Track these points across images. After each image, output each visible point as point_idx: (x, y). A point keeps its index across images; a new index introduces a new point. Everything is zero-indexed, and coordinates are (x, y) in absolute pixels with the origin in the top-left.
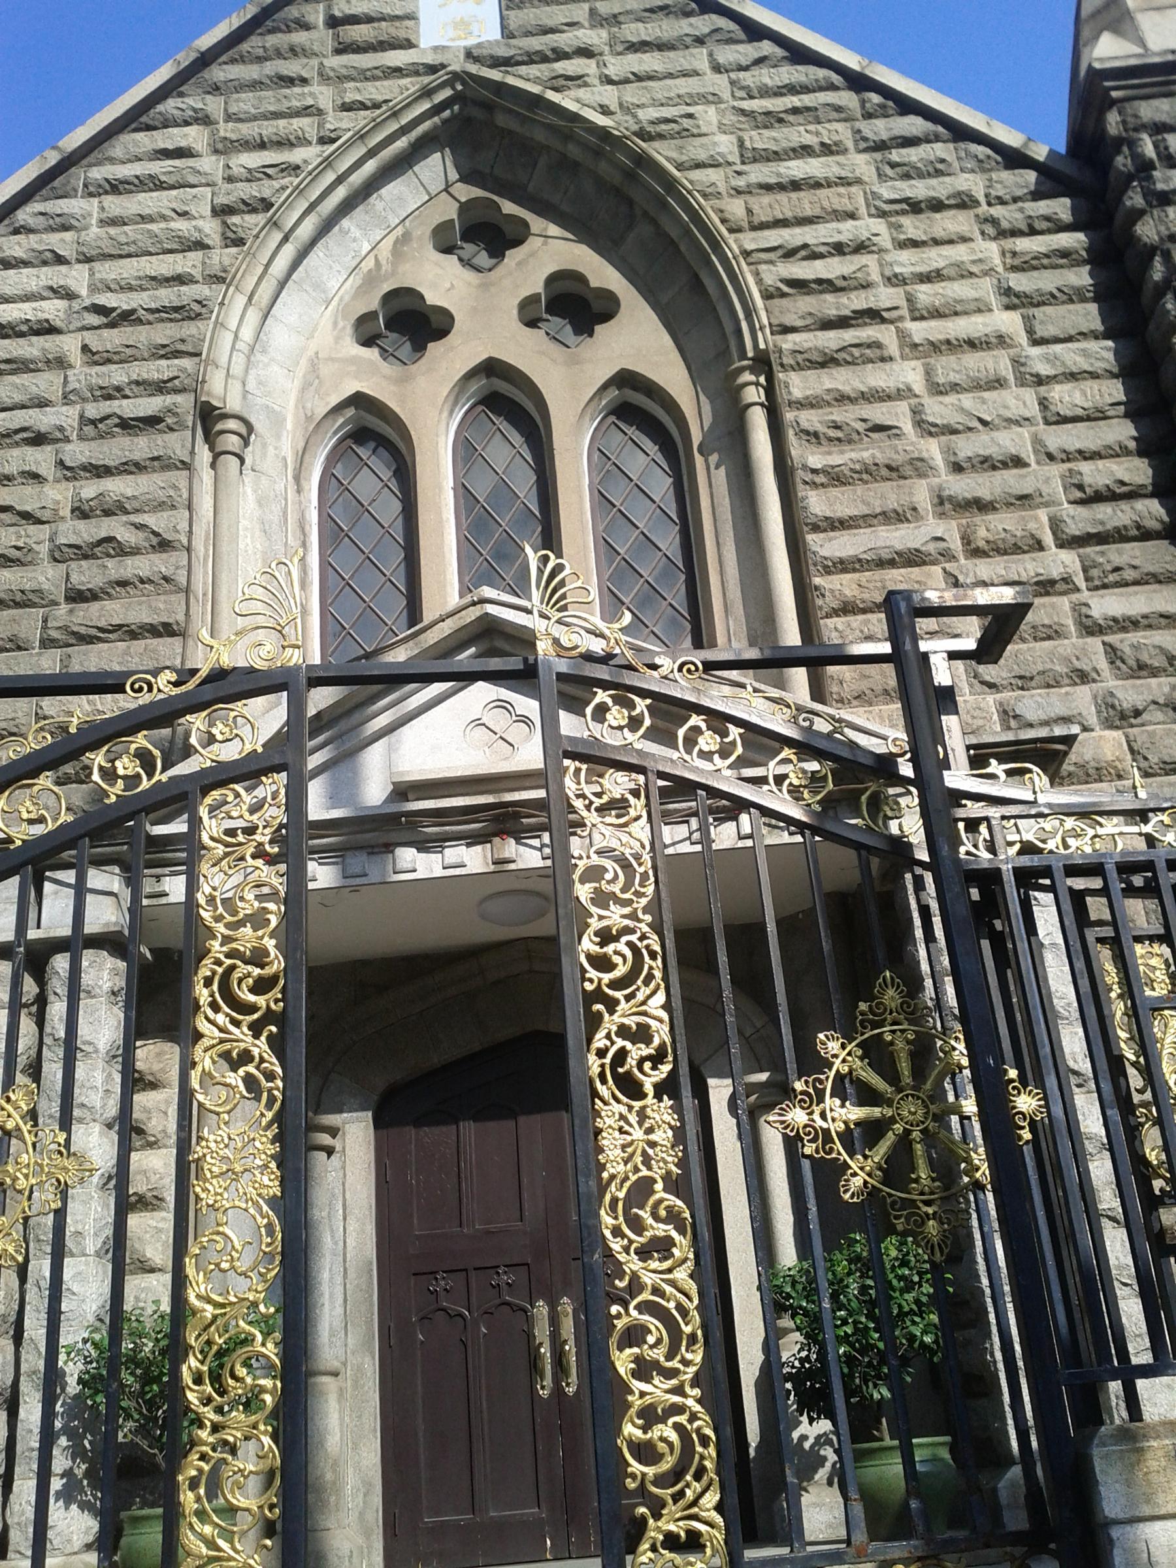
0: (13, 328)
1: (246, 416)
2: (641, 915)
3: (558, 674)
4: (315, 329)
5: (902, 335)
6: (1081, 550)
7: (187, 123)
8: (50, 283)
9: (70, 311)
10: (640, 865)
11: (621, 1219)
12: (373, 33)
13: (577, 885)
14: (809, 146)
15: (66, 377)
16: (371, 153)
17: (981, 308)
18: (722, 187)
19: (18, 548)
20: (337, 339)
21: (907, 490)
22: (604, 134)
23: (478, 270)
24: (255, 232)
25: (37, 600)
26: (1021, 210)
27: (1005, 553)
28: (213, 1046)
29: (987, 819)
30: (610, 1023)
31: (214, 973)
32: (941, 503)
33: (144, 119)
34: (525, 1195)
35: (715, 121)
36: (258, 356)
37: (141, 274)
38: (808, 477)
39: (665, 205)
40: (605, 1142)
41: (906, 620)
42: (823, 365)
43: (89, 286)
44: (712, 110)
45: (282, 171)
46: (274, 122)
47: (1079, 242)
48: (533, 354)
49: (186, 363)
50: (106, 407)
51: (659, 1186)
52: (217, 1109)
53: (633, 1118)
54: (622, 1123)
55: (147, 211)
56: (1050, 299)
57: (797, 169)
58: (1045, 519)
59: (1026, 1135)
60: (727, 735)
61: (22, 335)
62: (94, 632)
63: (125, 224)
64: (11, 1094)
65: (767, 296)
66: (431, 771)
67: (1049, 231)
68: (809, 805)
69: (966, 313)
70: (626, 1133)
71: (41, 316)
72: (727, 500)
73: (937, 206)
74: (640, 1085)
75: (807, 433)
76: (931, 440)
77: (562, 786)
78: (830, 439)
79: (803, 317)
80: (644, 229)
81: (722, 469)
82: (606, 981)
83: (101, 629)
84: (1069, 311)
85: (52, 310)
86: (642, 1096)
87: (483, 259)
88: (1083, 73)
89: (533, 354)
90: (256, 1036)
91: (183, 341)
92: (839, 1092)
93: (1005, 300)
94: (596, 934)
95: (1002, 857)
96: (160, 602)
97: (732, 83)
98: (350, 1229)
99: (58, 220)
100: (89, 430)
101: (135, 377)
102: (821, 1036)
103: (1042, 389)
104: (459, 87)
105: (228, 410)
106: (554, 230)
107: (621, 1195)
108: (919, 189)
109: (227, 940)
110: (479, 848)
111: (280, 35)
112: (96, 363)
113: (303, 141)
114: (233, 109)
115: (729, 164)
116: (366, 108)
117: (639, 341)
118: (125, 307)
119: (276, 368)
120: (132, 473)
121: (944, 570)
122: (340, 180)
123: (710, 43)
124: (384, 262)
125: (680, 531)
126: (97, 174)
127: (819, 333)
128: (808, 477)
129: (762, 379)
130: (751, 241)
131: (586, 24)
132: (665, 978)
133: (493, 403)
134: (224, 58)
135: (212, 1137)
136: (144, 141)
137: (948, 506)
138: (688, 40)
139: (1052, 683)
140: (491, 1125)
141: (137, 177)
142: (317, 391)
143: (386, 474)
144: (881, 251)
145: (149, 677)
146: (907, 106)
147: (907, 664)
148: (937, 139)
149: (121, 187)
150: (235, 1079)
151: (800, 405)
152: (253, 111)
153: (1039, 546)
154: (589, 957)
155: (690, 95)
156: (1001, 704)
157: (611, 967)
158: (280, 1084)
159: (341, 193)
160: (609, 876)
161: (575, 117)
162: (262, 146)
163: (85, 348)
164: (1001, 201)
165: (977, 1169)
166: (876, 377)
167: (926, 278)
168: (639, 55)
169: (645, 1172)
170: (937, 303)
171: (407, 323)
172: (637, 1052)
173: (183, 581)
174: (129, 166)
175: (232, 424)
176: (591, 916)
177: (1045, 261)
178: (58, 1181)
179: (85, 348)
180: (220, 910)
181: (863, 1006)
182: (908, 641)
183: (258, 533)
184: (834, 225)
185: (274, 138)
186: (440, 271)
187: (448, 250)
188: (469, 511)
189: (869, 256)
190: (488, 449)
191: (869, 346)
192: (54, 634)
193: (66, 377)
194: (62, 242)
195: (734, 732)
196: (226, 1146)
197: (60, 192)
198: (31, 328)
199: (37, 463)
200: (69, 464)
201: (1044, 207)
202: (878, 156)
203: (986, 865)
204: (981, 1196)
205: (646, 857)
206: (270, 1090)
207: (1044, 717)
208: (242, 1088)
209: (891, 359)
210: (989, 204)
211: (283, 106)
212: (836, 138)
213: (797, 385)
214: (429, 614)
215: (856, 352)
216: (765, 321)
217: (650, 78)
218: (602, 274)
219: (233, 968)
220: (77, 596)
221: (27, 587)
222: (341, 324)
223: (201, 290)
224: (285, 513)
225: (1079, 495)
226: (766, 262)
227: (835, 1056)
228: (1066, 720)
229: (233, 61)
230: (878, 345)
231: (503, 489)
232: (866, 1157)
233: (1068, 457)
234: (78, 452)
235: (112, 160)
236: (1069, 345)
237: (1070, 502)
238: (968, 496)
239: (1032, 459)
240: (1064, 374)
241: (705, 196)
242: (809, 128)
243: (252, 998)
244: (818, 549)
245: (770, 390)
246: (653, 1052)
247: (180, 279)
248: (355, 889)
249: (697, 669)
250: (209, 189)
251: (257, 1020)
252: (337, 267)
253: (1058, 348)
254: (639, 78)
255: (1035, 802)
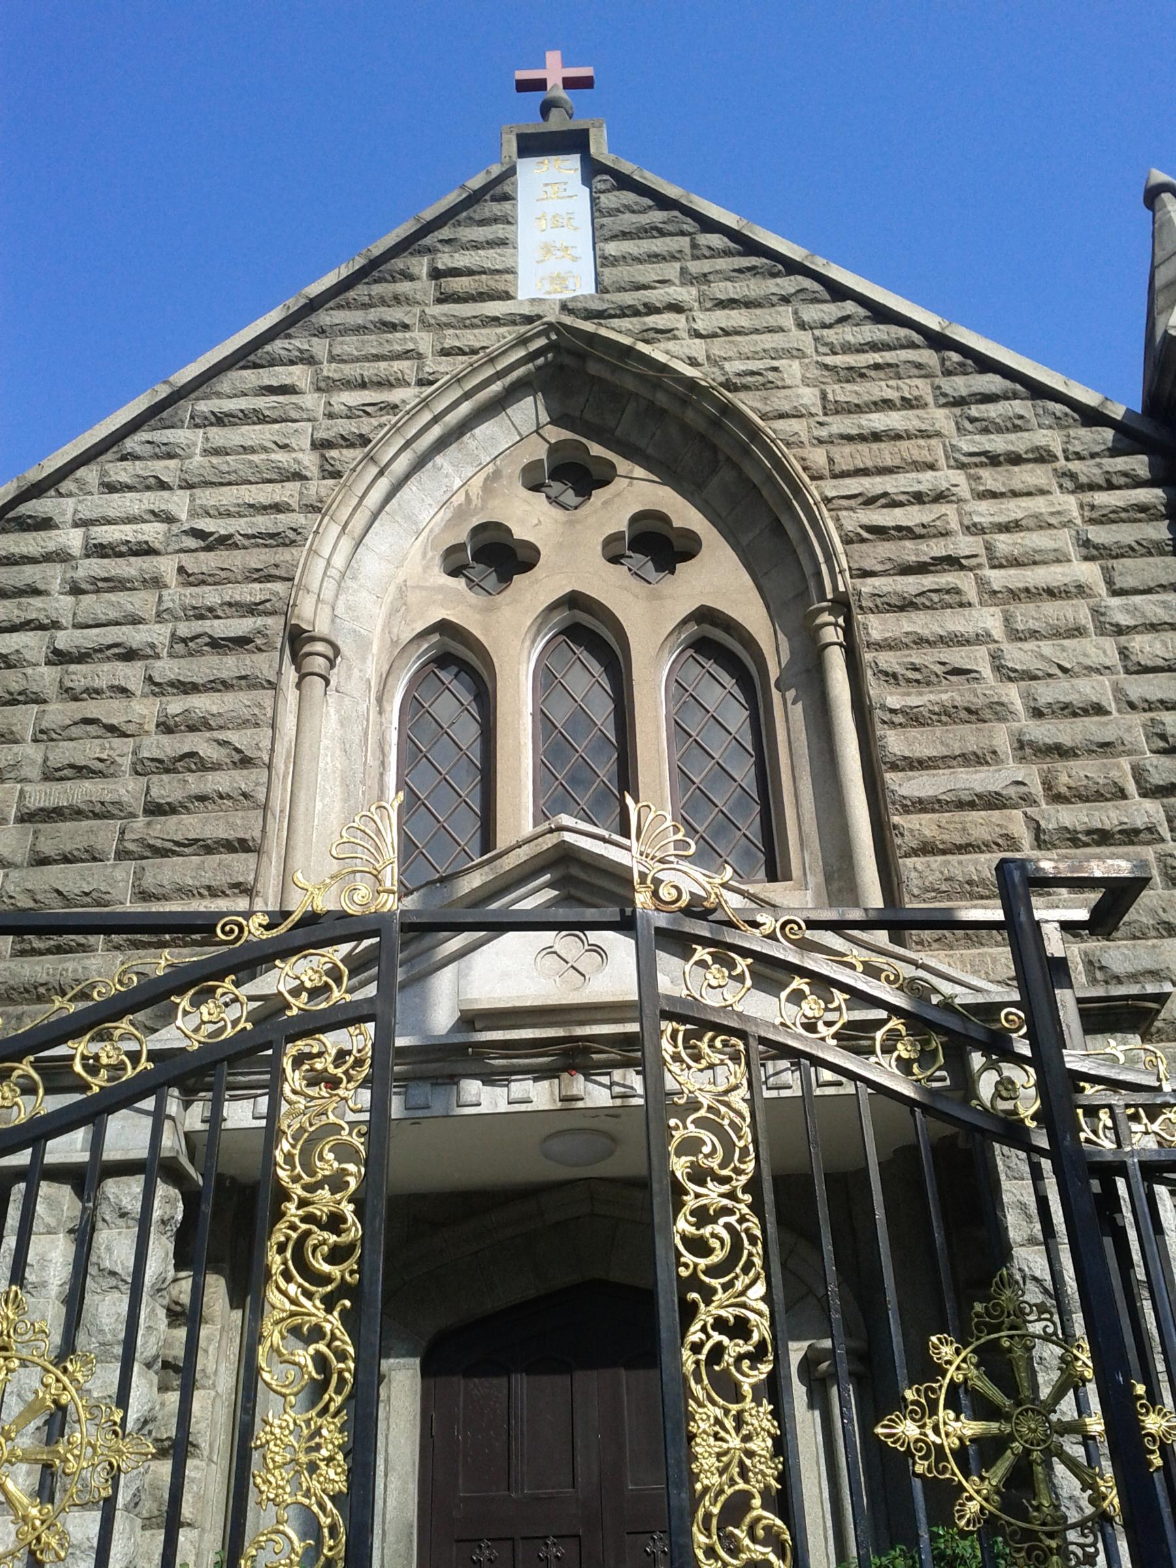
0: (113, 549)
1: (333, 638)
2: (740, 1195)
3: (657, 929)
4: (404, 558)
5: (981, 582)
6: (1165, 800)
7: (292, 363)
8: (152, 507)
9: (169, 535)
10: (740, 1138)
11: (715, 1537)
12: (474, 285)
13: (673, 1159)
14: (890, 400)
15: (160, 597)
16: (467, 396)
17: (1060, 559)
18: (804, 437)
19: (101, 760)
20: (426, 568)
21: (986, 733)
22: (692, 384)
23: (565, 507)
24: (352, 466)
25: (116, 812)
26: (1099, 465)
27: (1087, 800)
28: (283, 1320)
29: (1110, 1107)
30: (706, 1315)
31: (288, 1238)
32: (1022, 748)
33: (252, 358)
34: (579, 1459)
35: (799, 376)
36: (349, 583)
37: (240, 501)
38: (887, 717)
39: (747, 452)
40: (699, 1450)
41: (1020, 890)
42: (902, 609)
43: (189, 511)
44: (796, 364)
45: (381, 409)
46: (376, 364)
47: (1157, 497)
48: (617, 590)
49: (279, 587)
50: (198, 626)
51: (757, 1502)
52: (284, 1390)
53: (729, 1424)
54: (717, 1428)
55: (250, 443)
56: (1129, 551)
57: (878, 421)
58: (1128, 768)
59: (1157, 1460)
60: (832, 1001)
61: (121, 555)
62: (169, 845)
63: (227, 454)
64: (68, 1365)
65: (847, 541)
66: (500, 999)
67: (1127, 487)
68: (918, 1080)
69: (1045, 563)
70: (723, 1440)
71: (141, 538)
72: (804, 735)
73: (1015, 459)
74: (737, 1386)
75: (886, 674)
76: (1010, 685)
77: (658, 1048)
78: (909, 681)
79: (882, 562)
80: (727, 475)
81: (800, 705)
82: (702, 1267)
83: (177, 843)
84: (1148, 564)
85: (152, 532)
86: (738, 1398)
87: (570, 497)
88: (1158, 339)
89: (617, 590)
90: (329, 1310)
91: (276, 566)
92: (953, 1403)
93: (1084, 551)
94: (692, 1213)
95: (1128, 1149)
96: (238, 818)
97: (816, 339)
98: (391, 1487)
99: (163, 448)
100: (180, 648)
101: (228, 599)
102: (934, 1339)
103: (1123, 638)
104: (554, 337)
105: (316, 633)
106: (639, 472)
107: (715, 1510)
108: (998, 443)
109: (303, 1203)
110: (545, 1084)
111: (385, 285)
112: (191, 584)
113: (402, 382)
114: (337, 350)
115: (812, 415)
116: (464, 354)
117: (720, 579)
118: (223, 532)
119: (365, 594)
120: (219, 691)
121: (1025, 814)
122: (436, 420)
123: (796, 303)
124: (474, 498)
125: (755, 763)
126: (203, 407)
127: (898, 578)
128: (887, 717)
129: (841, 621)
130: (831, 488)
131: (677, 282)
132: (766, 1266)
133: (575, 633)
134: (331, 304)
135: (276, 1422)
136: (251, 378)
137: (1028, 751)
138: (775, 299)
139: (1138, 934)
140: (545, 1380)
141: (242, 411)
142: (404, 618)
143: (467, 698)
144: (960, 500)
145: (240, 919)
146: (986, 365)
147: (1019, 931)
148: (1015, 396)
149: (226, 420)
150: (304, 1356)
151: (879, 646)
152: (356, 353)
153: (1122, 794)
154: (684, 1238)
155: (775, 350)
156: (1086, 954)
157: (709, 1251)
158: (352, 1365)
159: (436, 431)
160: (706, 1149)
161: (664, 368)
162: (363, 385)
163: (181, 570)
164: (1079, 457)
165: (1104, 1498)
166: (954, 622)
167: (1005, 528)
168: (727, 311)
169: (741, 1485)
170: (1016, 552)
171: (495, 556)
172: (735, 1347)
173: (262, 797)
174: (234, 400)
175: (320, 647)
176: (687, 1193)
177: (1123, 515)
178: (111, 1464)
179: (181, 570)
180: (299, 1169)
181: (979, 1307)
182: (1022, 911)
183: (338, 752)
184: (914, 475)
185: (375, 379)
186: (528, 508)
187: (536, 488)
188: (546, 738)
189: (948, 506)
190: (567, 677)
191: (948, 592)
192: (131, 846)
193: (160, 597)
194: (167, 469)
195: (839, 997)
196: (291, 1433)
197: (168, 423)
198: (130, 549)
199: (127, 678)
200: (158, 680)
201: (1121, 463)
202: (957, 411)
203: (1110, 1158)
204: (1110, 1530)
205: (746, 1131)
206: (340, 1372)
207: (1131, 970)
208: (311, 1368)
209: (970, 605)
210: (1067, 459)
211: (385, 350)
212: (916, 393)
213: (876, 627)
214: (503, 840)
215: (935, 597)
216: (845, 566)
217: (738, 333)
218: (685, 515)
219: (308, 1233)
220: (156, 810)
221: (107, 799)
222: (430, 554)
223: (298, 519)
224: (366, 733)
225: (1162, 744)
226: (846, 509)
227: (949, 1362)
228: (1155, 974)
229: (339, 307)
230: (957, 591)
231: (581, 717)
232: (982, 1479)
233: (1150, 706)
234: (167, 669)
235: (219, 395)
236: (1149, 597)
237: (1153, 752)
238: (1048, 741)
239: (1113, 707)
240: (1144, 624)
241: (788, 444)
242: (891, 383)
243: (326, 1268)
244: (897, 788)
245: (848, 631)
246: (751, 1348)
247: (277, 508)
248: (416, 1121)
249: (800, 928)
250: (310, 424)
251: (332, 1292)
252: (428, 500)
253: (1137, 599)
254: (726, 333)
255: (1159, 1089)
